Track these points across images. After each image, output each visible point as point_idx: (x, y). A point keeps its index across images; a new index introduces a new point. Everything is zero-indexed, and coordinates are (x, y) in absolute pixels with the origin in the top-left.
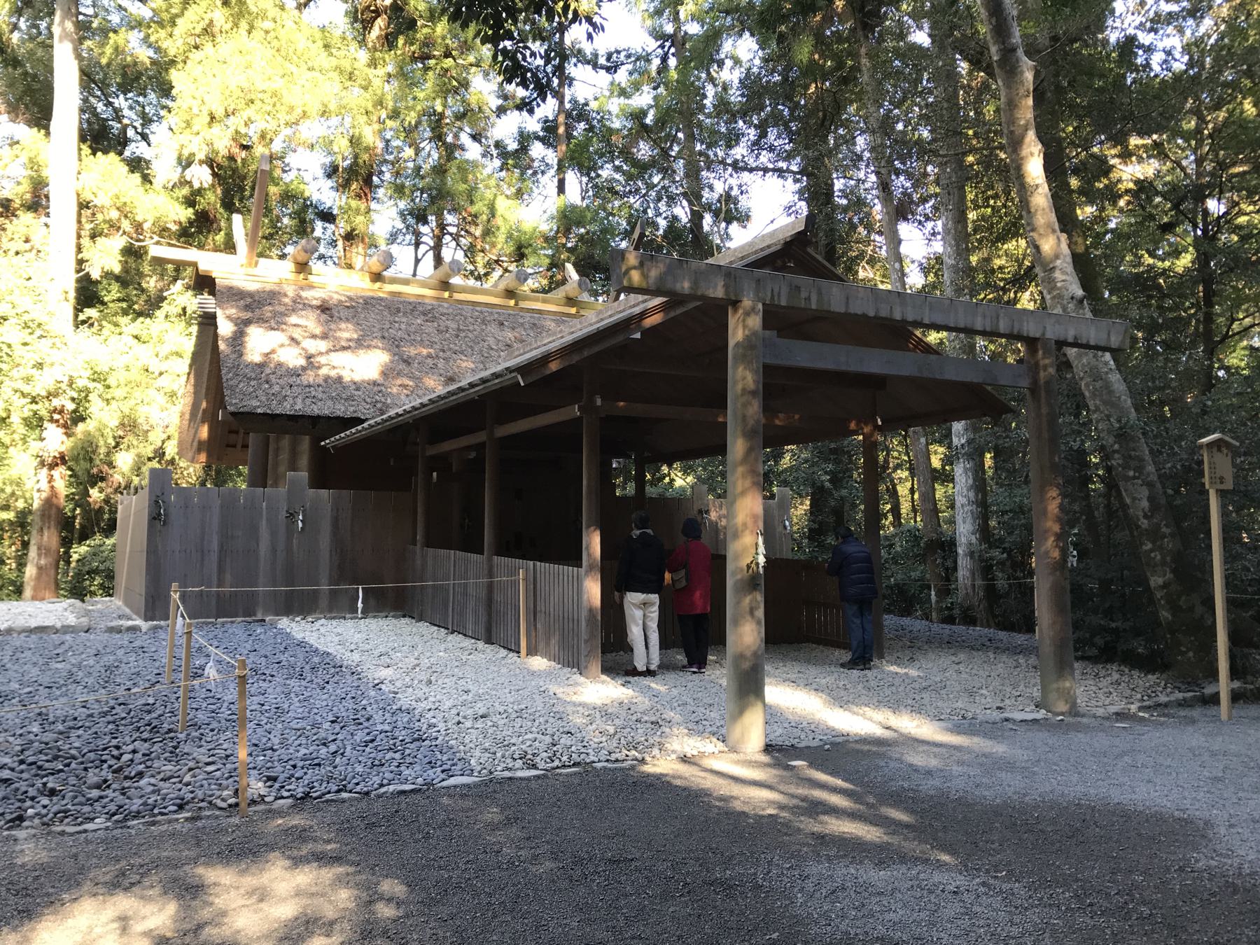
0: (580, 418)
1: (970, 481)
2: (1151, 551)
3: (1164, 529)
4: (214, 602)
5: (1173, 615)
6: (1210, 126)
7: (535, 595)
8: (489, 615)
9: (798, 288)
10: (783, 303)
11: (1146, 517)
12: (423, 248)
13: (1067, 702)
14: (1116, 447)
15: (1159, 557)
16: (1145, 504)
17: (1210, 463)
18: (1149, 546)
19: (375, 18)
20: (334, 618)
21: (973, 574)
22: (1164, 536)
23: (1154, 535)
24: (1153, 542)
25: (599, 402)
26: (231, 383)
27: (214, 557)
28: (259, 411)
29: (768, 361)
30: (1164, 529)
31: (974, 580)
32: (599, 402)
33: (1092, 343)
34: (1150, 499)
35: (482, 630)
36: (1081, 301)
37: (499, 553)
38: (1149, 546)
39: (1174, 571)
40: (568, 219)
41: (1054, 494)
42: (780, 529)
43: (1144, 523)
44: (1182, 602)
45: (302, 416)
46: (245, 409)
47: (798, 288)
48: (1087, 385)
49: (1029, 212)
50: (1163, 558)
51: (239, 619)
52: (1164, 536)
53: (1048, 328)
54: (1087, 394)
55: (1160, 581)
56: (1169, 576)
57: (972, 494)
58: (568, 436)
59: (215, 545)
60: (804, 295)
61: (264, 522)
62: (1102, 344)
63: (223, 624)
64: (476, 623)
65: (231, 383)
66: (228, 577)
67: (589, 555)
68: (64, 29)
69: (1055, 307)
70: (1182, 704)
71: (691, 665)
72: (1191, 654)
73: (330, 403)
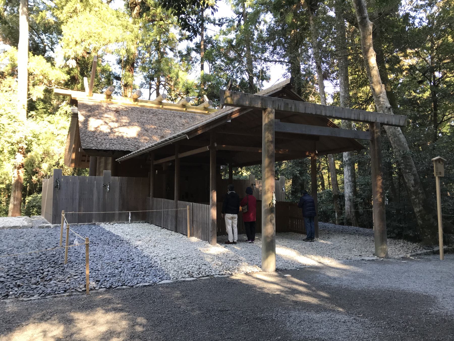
0: (209, 151)
1: (350, 174)
2: (415, 199)
3: (419, 191)
4: (77, 217)
5: (423, 222)
6: (436, 45)
7: (193, 215)
8: (176, 222)
9: (288, 104)
10: (282, 109)
11: (413, 186)
12: (152, 90)
13: (384, 253)
14: (402, 161)
15: (417, 201)
16: (413, 182)
17: (436, 167)
18: (414, 197)
19: (135, 7)
20: (120, 223)
21: (351, 207)
22: (419, 194)
23: (416, 193)
24: (416, 196)
25: (216, 145)
26: (83, 138)
27: (77, 201)
28: (93, 148)
29: (277, 130)
30: (419, 191)
31: (351, 209)
32: (216, 145)
33: (394, 124)
34: (414, 180)
35: (174, 227)
36: (389, 109)
37: (180, 200)
38: (414, 197)
39: (423, 206)
40: (205, 79)
41: (380, 178)
42: (281, 191)
43: (412, 189)
44: (426, 217)
45: (109, 150)
46: (88, 148)
47: (288, 104)
48: (392, 139)
49: (371, 76)
50: (419, 201)
51: (86, 223)
52: (419, 194)
53: (378, 119)
54: (392, 142)
55: (418, 210)
56: (421, 208)
57: (350, 178)
58: (205, 157)
59: (77, 197)
60: (290, 106)
61: (95, 188)
62: (397, 124)
63: (80, 225)
64: (172, 225)
65: (83, 138)
66: (82, 208)
67: (212, 200)
68: (23, 11)
69: (380, 111)
70: (426, 254)
71: (249, 240)
72: (429, 236)
73: (119, 145)
